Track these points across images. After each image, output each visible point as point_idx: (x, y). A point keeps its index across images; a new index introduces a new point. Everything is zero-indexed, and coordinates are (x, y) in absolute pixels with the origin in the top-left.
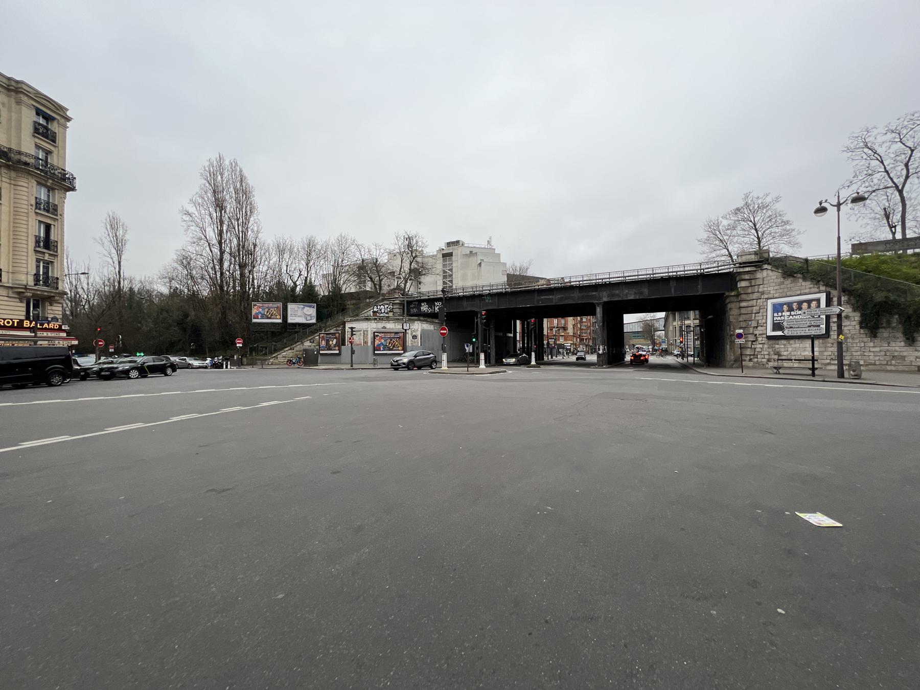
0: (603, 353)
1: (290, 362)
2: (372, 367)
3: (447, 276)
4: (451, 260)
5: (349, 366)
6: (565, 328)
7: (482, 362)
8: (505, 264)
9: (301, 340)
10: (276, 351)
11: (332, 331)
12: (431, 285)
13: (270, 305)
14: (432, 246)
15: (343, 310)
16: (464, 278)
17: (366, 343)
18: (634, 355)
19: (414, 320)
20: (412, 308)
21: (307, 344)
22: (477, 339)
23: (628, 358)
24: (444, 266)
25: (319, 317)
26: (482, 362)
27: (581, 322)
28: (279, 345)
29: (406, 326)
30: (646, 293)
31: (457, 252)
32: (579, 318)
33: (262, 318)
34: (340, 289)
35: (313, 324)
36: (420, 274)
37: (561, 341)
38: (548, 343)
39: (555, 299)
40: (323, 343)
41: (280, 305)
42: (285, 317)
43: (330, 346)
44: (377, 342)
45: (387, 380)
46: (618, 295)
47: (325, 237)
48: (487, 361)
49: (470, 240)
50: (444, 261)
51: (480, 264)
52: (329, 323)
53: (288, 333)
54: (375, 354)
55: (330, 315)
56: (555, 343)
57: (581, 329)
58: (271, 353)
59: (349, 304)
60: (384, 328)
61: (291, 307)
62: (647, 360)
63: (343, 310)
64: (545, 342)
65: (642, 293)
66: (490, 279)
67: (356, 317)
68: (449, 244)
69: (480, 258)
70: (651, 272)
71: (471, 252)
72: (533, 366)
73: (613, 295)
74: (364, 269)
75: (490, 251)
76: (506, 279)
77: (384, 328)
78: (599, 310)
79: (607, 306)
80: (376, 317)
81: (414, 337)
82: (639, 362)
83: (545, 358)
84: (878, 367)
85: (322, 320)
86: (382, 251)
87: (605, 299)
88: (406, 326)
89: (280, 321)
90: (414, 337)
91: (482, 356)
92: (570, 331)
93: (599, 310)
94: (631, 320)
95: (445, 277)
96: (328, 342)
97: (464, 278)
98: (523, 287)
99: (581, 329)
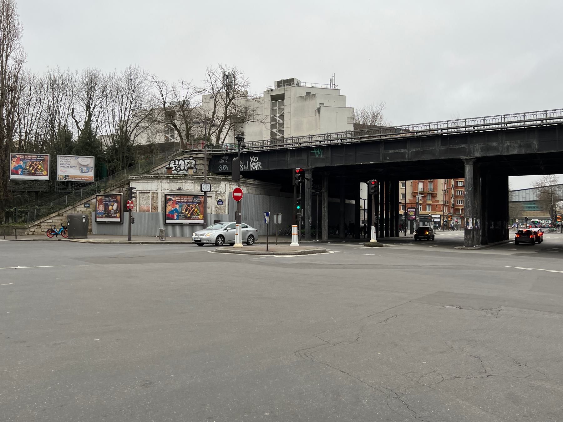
0: (474, 229)
1: (51, 232)
2: (157, 240)
3: (277, 125)
4: (282, 104)
5: (126, 240)
6: (433, 195)
7: (295, 237)
8: (352, 110)
9: (72, 203)
10: (39, 217)
11: (114, 193)
12: (257, 134)
13: (34, 157)
14: (257, 84)
15: (130, 165)
16: (298, 127)
17: (155, 208)
18: (520, 233)
19: (220, 180)
20: (221, 164)
21: (81, 209)
22: (303, 207)
23: (512, 235)
24: (273, 111)
25: (99, 173)
26: (295, 237)
27: (456, 187)
28: (43, 210)
29: (206, 188)
30: (535, 145)
31: (290, 93)
32: (453, 182)
33: (23, 174)
34: (127, 139)
35: (90, 183)
36: (243, 120)
37: (428, 211)
38: (406, 214)
39: (408, 154)
40: (101, 208)
41: (47, 157)
42: (53, 173)
43: (109, 212)
44: (169, 208)
45: (125, 262)
46: (496, 149)
47: (112, 69)
48: (302, 237)
49: (309, 79)
50: (273, 105)
51: (319, 110)
52: (111, 181)
53: (61, 192)
54: (166, 224)
55: (113, 172)
56: (416, 213)
57: (456, 197)
58: (33, 220)
59: (141, 160)
60: (180, 189)
61: (61, 159)
62: (539, 239)
63: (130, 165)
64: (401, 212)
65: (529, 146)
66: (333, 126)
67: (148, 174)
68: (280, 84)
69: (316, 103)
70: (543, 116)
71: (308, 94)
72: (373, 245)
73: (488, 149)
74: (175, 114)
75: (333, 93)
76: (352, 128)
77: (180, 189)
78: (468, 169)
79: (479, 163)
80: (171, 176)
81: (220, 202)
82: (529, 242)
83: (401, 234)
84: (4, 65)
85: (101, 178)
86: (191, 90)
87: (478, 154)
88: (206, 188)
89: (47, 178)
90: (220, 202)
91: (295, 229)
92: (440, 198)
93: (468, 169)
94: (520, 185)
95: (273, 126)
96: (106, 206)
97: (298, 127)
98: (365, 138)
99: (456, 197)
